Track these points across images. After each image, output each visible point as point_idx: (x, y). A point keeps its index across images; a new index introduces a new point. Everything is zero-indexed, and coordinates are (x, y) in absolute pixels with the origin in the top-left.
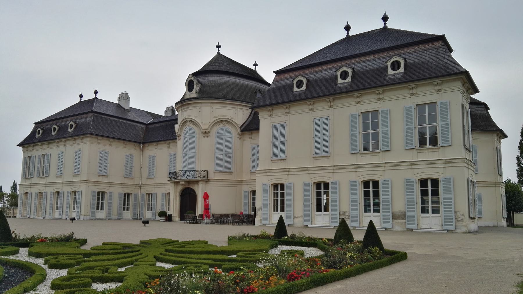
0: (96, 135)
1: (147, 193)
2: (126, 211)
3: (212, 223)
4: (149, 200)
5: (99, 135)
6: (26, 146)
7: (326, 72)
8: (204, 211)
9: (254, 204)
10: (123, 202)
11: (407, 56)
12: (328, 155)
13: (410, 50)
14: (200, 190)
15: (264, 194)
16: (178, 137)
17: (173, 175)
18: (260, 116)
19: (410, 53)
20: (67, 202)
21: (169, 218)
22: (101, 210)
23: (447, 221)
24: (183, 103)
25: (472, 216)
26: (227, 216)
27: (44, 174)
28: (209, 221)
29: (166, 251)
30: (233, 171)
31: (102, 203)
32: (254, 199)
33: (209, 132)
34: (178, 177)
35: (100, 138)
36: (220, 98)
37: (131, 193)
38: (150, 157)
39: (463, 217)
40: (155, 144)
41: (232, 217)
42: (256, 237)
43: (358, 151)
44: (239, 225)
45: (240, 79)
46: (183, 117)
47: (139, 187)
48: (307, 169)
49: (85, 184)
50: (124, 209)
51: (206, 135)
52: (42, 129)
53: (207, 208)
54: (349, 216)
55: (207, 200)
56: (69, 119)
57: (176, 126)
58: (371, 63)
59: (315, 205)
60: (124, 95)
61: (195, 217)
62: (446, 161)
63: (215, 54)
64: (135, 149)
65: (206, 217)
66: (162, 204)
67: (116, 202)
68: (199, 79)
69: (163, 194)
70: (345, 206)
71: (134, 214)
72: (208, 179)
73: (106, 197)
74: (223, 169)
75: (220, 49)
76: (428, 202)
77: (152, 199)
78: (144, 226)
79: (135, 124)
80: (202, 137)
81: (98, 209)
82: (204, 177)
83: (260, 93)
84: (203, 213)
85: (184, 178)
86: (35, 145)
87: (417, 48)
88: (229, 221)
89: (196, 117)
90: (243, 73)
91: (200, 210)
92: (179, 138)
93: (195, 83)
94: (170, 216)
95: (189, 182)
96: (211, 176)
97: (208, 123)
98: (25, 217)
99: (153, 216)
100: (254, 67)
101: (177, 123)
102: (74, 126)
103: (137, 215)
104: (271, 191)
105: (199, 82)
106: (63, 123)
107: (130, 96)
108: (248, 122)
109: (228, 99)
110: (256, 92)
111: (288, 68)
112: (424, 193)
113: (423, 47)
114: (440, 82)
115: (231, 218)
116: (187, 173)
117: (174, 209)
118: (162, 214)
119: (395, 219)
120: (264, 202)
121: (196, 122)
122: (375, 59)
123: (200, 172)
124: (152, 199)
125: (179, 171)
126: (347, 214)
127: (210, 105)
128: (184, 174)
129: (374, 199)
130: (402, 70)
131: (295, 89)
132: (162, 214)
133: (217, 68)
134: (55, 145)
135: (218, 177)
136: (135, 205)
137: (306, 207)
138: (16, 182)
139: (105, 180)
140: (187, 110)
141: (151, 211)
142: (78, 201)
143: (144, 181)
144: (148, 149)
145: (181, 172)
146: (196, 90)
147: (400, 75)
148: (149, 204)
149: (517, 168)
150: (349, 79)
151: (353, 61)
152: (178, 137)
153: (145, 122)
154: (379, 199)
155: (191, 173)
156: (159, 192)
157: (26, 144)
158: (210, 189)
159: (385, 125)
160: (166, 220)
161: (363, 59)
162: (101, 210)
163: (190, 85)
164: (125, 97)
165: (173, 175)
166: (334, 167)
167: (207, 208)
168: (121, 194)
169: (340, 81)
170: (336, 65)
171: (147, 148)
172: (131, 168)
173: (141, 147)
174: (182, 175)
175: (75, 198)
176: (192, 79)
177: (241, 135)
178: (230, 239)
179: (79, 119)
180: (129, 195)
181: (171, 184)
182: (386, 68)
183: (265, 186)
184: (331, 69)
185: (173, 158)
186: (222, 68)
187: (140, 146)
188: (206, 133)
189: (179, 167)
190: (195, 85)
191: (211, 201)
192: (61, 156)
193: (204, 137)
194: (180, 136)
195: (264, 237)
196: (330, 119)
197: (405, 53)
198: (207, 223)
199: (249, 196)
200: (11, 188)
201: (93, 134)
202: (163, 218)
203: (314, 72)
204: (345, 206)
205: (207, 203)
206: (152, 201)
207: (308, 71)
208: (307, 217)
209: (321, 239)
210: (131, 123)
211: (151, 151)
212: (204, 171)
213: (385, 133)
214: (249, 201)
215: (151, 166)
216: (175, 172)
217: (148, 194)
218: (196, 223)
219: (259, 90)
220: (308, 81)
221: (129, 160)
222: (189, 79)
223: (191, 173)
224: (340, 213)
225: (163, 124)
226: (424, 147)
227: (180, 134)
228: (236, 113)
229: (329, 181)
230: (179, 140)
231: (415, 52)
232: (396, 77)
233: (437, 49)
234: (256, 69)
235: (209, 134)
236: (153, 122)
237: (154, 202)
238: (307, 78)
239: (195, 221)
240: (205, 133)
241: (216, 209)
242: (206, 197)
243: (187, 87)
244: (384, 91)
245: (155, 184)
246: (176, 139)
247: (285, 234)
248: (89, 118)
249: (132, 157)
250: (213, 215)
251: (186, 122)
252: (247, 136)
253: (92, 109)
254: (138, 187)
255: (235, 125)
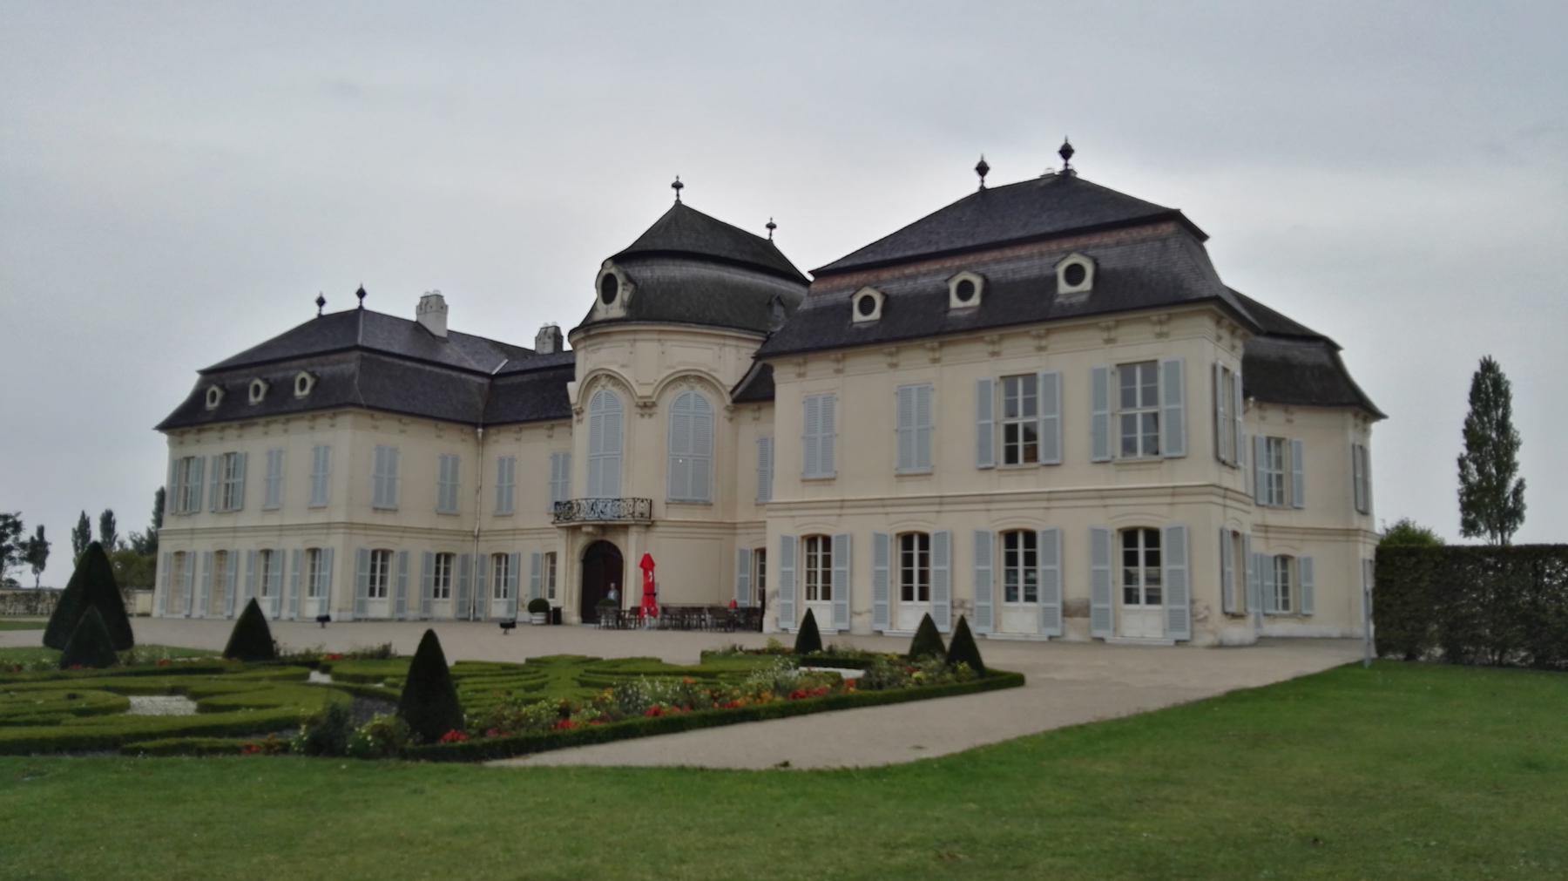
0: (369, 407)
1: (494, 552)
2: (440, 598)
3: (662, 628)
4: (498, 570)
5: (377, 408)
6: (178, 431)
7: (924, 279)
8: (643, 599)
9: (762, 582)
10: (368, 574)
11: (1100, 253)
12: (927, 470)
13: (1108, 238)
14: (631, 549)
15: (786, 558)
16: (578, 414)
17: (563, 510)
18: (778, 375)
19: (1106, 246)
20: (294, 578)
21: (555, 617)
22: (381, 594)
23: (1175, 621)
24: (588, 330)
25: (1232, 609)
26: (698, 610)
27: (231, 500)
28: (654, 622)
29: (586, 671)
30: (713, 501)
31: (382, 578)
32: (763, 569)
33: (654, 405)
34: (577, 515)
35: (378, 415)
36: (680, 320)
37: (391, 548)
38: (501, 461)
39: (1206, 613)
40: (515, 428)
41: (710, 613)
42: (758, 652)
43: (992, 465)
44: (726, 631)
45: (732, 270)
46: (590, 366)
47: (474, 536)
48: (882, 503)
49: (342, 530)
50: (436, 595)
51: (647, 411)
52: (222, 387)
53: (650, 592)
54: (971, 610)
55: (651, 573)
56: (295, 363)
57: (572, 388)
58: (1024, 264)
59: (1120, 586)
60: (433, 300)
61: (619, 616)
62: (1175, 491)
63: (669, 204)
64: (463, 440)
65: (649, 613)
66: (534, 582)
67: (417, 575)
68: (630, 271)
69: (535, 556)
70: (964, 588)
71: (462, 607)
72: (652, 519)
73: (393, 564)
74: (689, 496)
75: (681, 191)
76: (1137, 580)
77: (506, 569)
78: (505, 633)
79: (464, 376)
80: (638, 416)
81: (372, 593)
82: (642, 515)
83: (782, 304)
84: (639, 604)
85: (592, 516)
86: (204, 430)
87: (1123, 235)
88: (703, 623)
89: (623, 366)
90: (738, 257)
91: (632, 595)
92: (580, 417)
93: (620, 282)
94: (557, 611)
95: (604, 528)
96: (660, 512)
97: (652, 381)
98: (177, 616)
99: (509, 610)
100: (768, 231)
101: (573, 379)
102: (310, 383)
103: (469, 608)
104: (800, 553)
105: (629, 279)
106: (280, 375)
107: (447, 301)
108: (750, 378)
109: (700, 323)
110: (770, 304)
111: (836, 266)
112: (1130, 559)
113: (1135, 233)
114: (1164, 317)
115: (708, 616)
116: (601, 506)
117: (567, 595)
118: (538, 606)
119: (1070, 616)
120: (786, 578)
121: (623, 380)
122: (1031, 257)
123: (632, 503)
124: (506, 569)
125: (579, 501)
126: (968, 606)
127: (655, 336)
128: (592, 509)
129: (1026, 572)
130: (1087, 285)
131: (858, 317)
132: (538, 606)
133: (676, 245)
134: (259, 430)
135: (676, 515)
136: (464, 587)
137: (880, 589)
138: (87, 514)
139: (389, 520)
140: (599, 349)
141: (506, 600)
142: (323, 573)
143: (486, 523)
144: (496, 441)
145: (584, 502)
146: (622, 301)
147: (1083, 298)
148: (498, 581)
149: (1460, 487)
150: (975, 300)
151: (987, 256)
152: (578, 414)
153: (487, 371)
154: (1034, 571)
155: (609, 505)
156: (526, 550)
157: (182, 423)
158: (659, 545)
159: (1050, 408)
160: (548, 622)
161: (1009, 253)
162: (381, 594)
163: (607, 287)
164: (434, 304)
165: (563, 510)
166: (941, 500)
167: (650, 592)
168: (428, 555)
169: (955, 302)
170: (948, 263)
171: (494, 438)
172: (454, 488)
173: (480, 435)
174: (588, 509)
175: (266, 567)
176: (613, 271)
177: (732, 412)
178: (704, 655)
179: (323, 365)
180: (448, 557)
181: (559, 531)
182: (1054, 279)
183: (786, 541)
184: (938, 272)
185: (562, 464)
186: (688, 244)
187: (476, 433)
188: (647, 407)
189: (579, 491)
190: (620, 289)
191: (660, 575)
192: (275, 458)
193: (642, 416)
194: (583, 411)
195: (774, 651)
196: (933, 390)
197: (1097, 246)
198: (650, 628)
199: (752, 563)
200: (75, 532)
201: (360, 406)
202: (539, 617)
203: (899, 279)
204: (964, 588)
205: (651, 580)
206: (506, 574)
207: (886, 275)
208: (880, 613)
209: (886, 655)
210: (454, 374)
211: (506, 445)
212: (642, 501)
213: (1050, 424)
214: (751, 575)
215: (506, 484)
216: (569, 502)
217: (498, 556)
218: (625, 627)
219: (778, 298)
220: (887, 299)
221: (449, 468)
222: (605, 272)
223: (609, 505)
224: (952, 602)
225: (535, 376)
226: (1130, 458)
227: (581, 408)
228: (720, 357)
229: (930, 530)
230: (579, 421)
231: (1118, 244)
232: (1074, 300)
233: (1164, 240)
234: (772, 238)
235: (654, 410)
236: (506, 370)
237: (512, 577)
238: (883, 294)
239: (621, 622)
240: (645, 406)
241: (671, 593)
242: (647, 564)
243: (600, 290)
244: (1049, 332)
245: (515, 531)
246: (570, 417)
247: (817, 644)
248: (350, 365)
249: (456, 460)
250: (665, 610)
251: (596, 379)
252: (747, 415)
253: (356, 339)
254: (471, 538)
255: (718, 386)
